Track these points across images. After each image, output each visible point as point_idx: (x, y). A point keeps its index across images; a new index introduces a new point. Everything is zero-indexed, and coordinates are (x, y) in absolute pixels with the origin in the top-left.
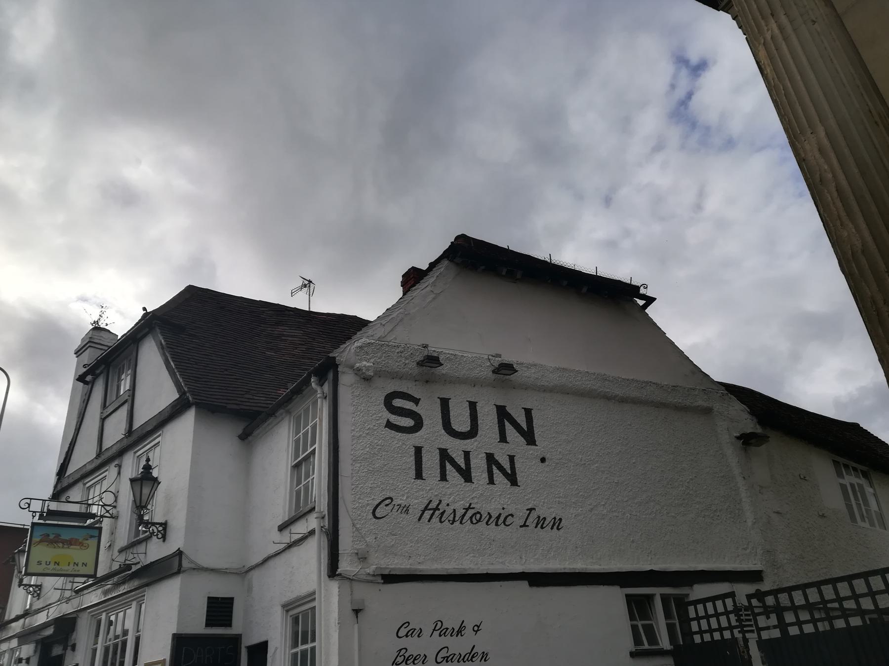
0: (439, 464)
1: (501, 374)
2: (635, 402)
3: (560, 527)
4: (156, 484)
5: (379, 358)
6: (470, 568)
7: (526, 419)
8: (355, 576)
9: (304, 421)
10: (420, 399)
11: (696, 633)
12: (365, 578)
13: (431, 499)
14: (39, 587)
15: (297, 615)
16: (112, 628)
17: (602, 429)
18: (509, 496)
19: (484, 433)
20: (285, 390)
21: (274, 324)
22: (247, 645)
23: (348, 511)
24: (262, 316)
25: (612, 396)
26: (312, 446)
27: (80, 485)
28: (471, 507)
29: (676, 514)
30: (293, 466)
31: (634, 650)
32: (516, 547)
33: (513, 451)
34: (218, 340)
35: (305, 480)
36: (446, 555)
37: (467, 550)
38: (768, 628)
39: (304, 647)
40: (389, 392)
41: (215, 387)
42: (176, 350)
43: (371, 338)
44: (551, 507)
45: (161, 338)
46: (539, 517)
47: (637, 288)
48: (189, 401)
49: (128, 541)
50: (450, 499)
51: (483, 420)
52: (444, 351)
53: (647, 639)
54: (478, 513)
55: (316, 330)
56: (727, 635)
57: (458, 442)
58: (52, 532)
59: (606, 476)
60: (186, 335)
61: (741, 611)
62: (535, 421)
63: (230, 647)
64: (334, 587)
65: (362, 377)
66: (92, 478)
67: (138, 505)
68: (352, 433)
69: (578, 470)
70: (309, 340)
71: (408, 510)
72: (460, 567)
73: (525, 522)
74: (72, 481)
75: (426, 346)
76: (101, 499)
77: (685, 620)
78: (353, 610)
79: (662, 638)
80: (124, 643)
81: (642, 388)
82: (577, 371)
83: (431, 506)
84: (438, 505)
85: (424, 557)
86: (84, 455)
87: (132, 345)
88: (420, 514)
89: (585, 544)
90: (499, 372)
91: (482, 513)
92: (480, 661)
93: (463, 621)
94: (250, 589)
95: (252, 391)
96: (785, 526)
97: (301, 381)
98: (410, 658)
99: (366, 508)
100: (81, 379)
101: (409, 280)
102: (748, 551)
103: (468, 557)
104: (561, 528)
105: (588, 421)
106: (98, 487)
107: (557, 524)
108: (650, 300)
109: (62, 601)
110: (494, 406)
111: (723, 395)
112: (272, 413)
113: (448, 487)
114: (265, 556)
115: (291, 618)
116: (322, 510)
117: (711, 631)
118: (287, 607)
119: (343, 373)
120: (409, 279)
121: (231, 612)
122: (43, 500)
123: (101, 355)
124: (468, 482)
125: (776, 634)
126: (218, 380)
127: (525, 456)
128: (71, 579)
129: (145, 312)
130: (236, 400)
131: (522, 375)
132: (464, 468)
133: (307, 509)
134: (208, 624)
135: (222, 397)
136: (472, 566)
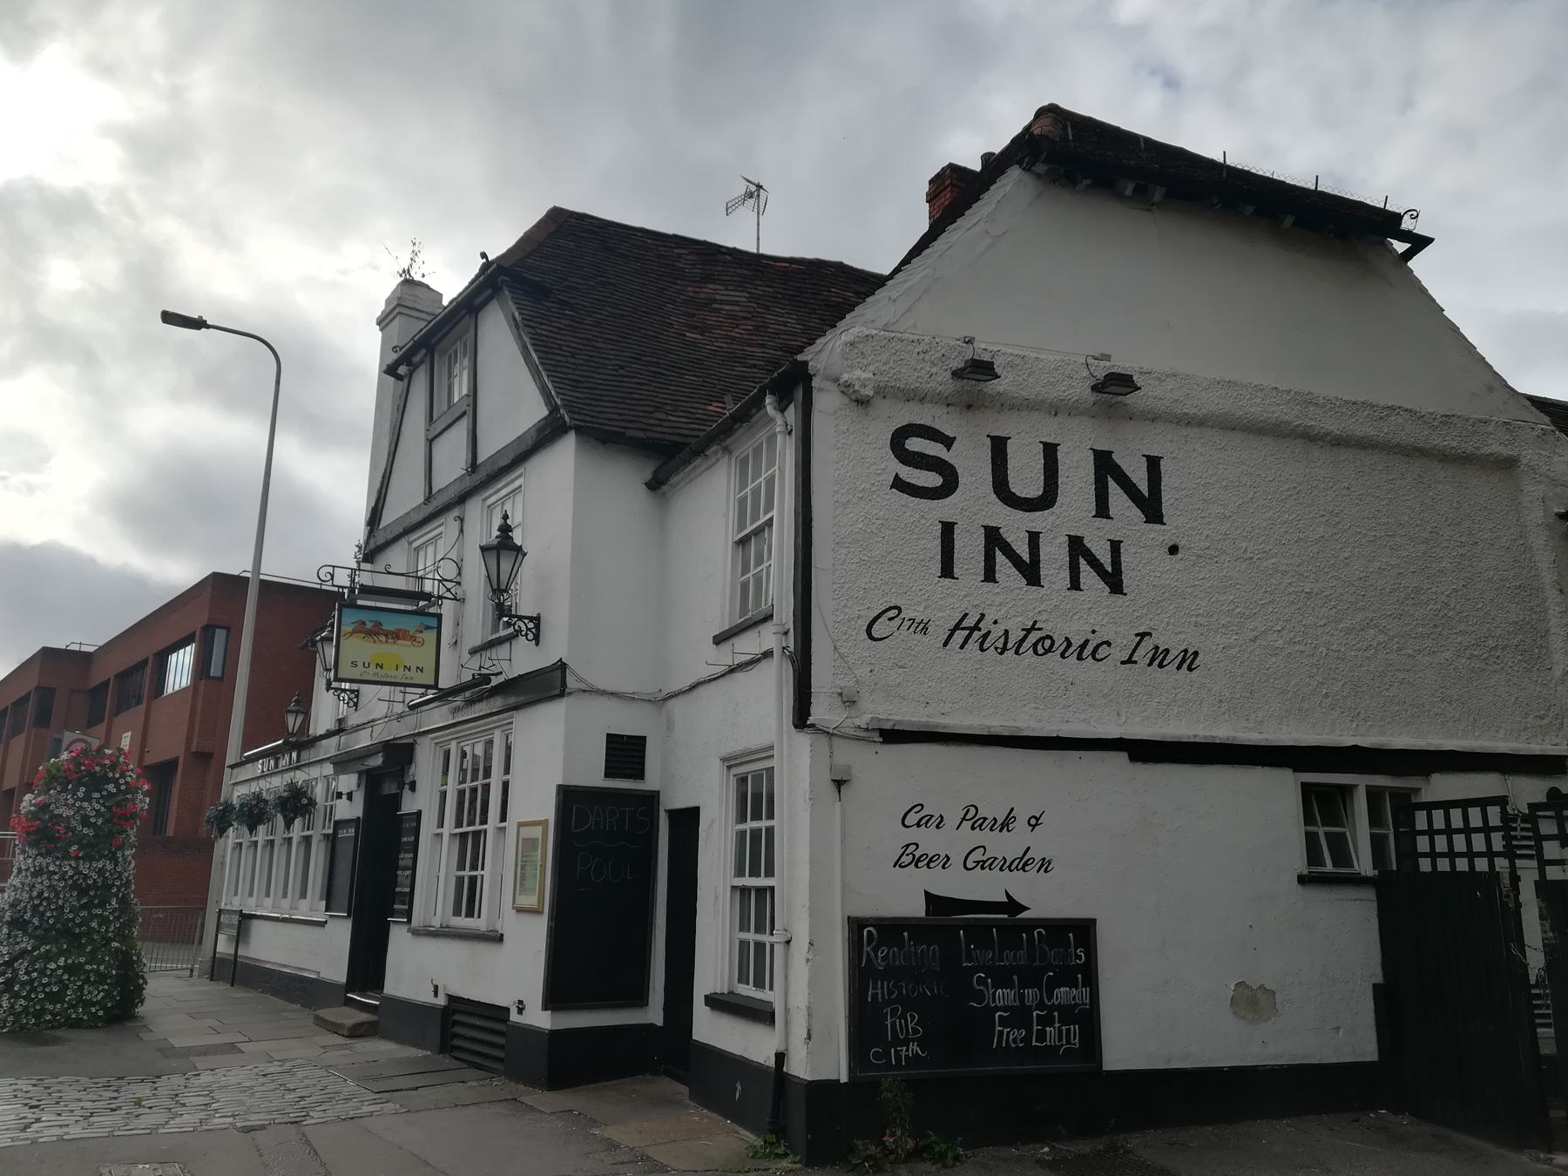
3: (1193, 666)
4: (520, 556)
5: (885, 364)
6: (1029, 726)
7: (1148, 477)
10: (955, 438)
11: (1424, 855)
19: (1068, 500)
21: (698, 279)
22: (667, 808)
23: (826, 627)
25: (1318, 433)
26: (766, 512)
27: (403, 542)
29: (1415, 651)
31: (1305, 872)
32: (1112, 697)
33: (1119, 533)
34: (606, 310)
35: (755, 567)
37: (1026, 697)
39: (756, 824)
42: (539, 331)
44: (1181, 633)
45: (513, 307)
46: (1157, 648)
47: (1398, 218)
48: (565, 422)
49: (482, 640)
51: (1068, 476)
52: (1004, 350)
56: (1482, 865)
57: (1019, 514)
58: (368, 618)
59: (1290, 581)
60: (553, 302)
62: (1165, 480)
64: (803, 740)
65: (854, 397)
67: (495, 587)
68: (833, 496)
69: (1238, 569)
71: (927, 629)
72: (1011, 725)
73: (1132, 655)
75: (969, 341)
76: (437, 570)
77: (1407, 836)
80: (487, 787)
81: (1382, 418)
82: (1256, 386)
83: (967, 623)
84: (979, 621)
85: (950, 705)
86: (406, 499)
89: (1238, 696)
90: (1105, 390)
91: (1054, 638)
92: (1038, 871)
93: (1012, 809)
94: (670, 726)
95: (666, 407)
97: (747, 401)
99: (856, 622)
100: (390, 370)
102: (1546, 721)
106: (430, 550)
107: (1189, 660)
108: (1420, 243)
110: (1091, 451)
111: (1544, 434)
112: (699, 451)
118: (730, 762)
119: (821, 390)
120: (942, 187)
122: (352, 569)
123: (419, 333)
128: (402, 689)
130: (641, 422)
134: (609, 774)
136: (1033, 724)
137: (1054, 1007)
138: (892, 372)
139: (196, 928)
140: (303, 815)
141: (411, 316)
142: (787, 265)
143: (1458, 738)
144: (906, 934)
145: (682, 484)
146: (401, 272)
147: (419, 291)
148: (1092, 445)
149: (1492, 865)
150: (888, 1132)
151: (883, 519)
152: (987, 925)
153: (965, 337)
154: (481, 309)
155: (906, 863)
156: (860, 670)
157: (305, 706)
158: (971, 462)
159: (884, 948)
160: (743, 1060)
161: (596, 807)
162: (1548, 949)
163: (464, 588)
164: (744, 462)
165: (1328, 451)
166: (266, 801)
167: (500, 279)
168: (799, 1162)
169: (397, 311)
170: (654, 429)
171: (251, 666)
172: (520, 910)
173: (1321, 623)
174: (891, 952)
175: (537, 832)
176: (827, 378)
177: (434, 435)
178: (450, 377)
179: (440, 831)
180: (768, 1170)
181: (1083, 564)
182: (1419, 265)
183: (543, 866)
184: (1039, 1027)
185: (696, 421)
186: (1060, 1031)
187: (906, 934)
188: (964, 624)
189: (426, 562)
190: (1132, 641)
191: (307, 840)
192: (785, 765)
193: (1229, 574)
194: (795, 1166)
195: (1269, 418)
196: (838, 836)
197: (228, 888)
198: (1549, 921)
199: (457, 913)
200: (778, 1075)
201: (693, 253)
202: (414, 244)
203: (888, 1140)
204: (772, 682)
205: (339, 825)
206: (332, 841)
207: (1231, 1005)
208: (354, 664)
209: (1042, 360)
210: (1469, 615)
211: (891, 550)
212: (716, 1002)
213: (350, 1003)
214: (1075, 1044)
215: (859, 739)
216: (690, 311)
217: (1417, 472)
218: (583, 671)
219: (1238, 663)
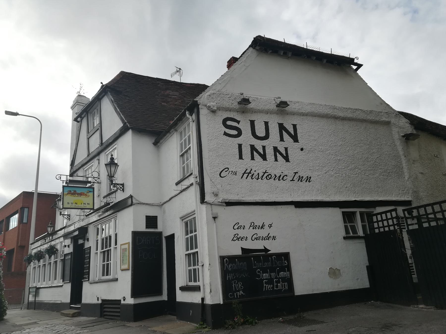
1: (281, 107)
3: (310, 181)
4: (117, 166)
9: (184, 134)
10: (240, 121)
11: (376, 228)
12: (217, 203)
14: (69, 215)
15: (187, 221)
16: (104, 232)
20: (169, 124)
24: (158, 85)
27: (82, 169)
31: (345, 236)
35: (186, 162)
36: (255, 194)
38: (412, 224)
39: (191, 235)
41: (139, 120)
43: (215, 90)
44: (306, 172)
45: (111, 97)
46: (300, 176)
47: (353, 59)
48: (128, 127)
50: (256, 169)
51: (272, 131)
53: (351, 231)
54: (270, 174)
55: (185, 92)
56: (392, 228)
57: (259, 141)
58: (72, 190)
61: (400, 219)
62: (298, 131)
63: (157, 237)
64: (204, 207)
65: (211, 110)
66: (87, 166)
67: (110, 175)
68: (207, 138)
70: (182, 97)
71: (236, 174)
74: (78, 168)
75: (242, 94)
77: (371, 222)
78: (213, 217)
81: (354, 112)
84: (251, 171)
85: (244, 195)
86: (82, 156)
87: (98, 102)
92: (272, 240)
93: (264, 223)
94: (164, 212)
96: (425, 180)
97: (181, 114)
98: (240, 238)
100: (75, 120)
101: (231, 64)
102: (405, 191)
106: (90, 170)
107: (309, 179)
108: (359, 66)
109: (80, 221)
115: (184, 223)
117: (384, 227)
118: (182, 218)
119: (202, 108)
120: (231, 63)
121: (157, 222)
122: (66, 175)
125: (416, 227)
129: (102, 85)
132: (263, 154)
133: (189, 174)
134: (147, 227)
135: (143, 125)
136: (267, 198)
137: (280, 278)
139: (22, 299)
140: (54, 255)
141: (81, 105)
142: (189, 85)
143: (382, 197)
144: (236, 260)
145: (164, 142)
146: (77, 92)
147: (82, 98)
148: (278, 122)
149: (394, 228)
150: (235, 317)
151: (222, 144)
152: (259, 256)
153: (241, 93)
154: (102, 99)
156: (218, 186)
157: (53, 224)
158: (245, 127)
159: (230, 264)
160: (192, 303)
161: (144, 237)
162: (412, 248)
163: (101, 179)
164: (181, 133)
165: (341, 121)
166: (42, 252)
167: (107, 90)
168: (210, 329)
169: (76, 104)
170: (154, 128)
171: (36, 214)
172: (122, 270)
173: (343, 168)
174: (233, 265)
175: (126, 246)
176: (203, 105)
177: (89, 137)
178: (93, 120)
179: (97, 252)
180: (201, 331)
181: (278, 154)
182: (360, 72)
184: (276, 284)
185: (167, 126)
186: (282, 285)
187: (236, 260)
188: (246, 172)
190: (293, 175)
191: (56, 262)
192: (199, 215)
193: (317, 155)
194: (209, 330)
195: (325, 113)
196: (215, 233)
197: (32, 281)
198: (411, 241)
199: (103, 275)
200: (203, 305)
201: (162, 82)
202: (81, 84)
203: (236, 319)
204: (194, 192)
205: (66, 255)
206: (63, 261)
207: (328, 275)
208: (68, 203)
209: (262, 99)
210: (382, 164)
212: (183, 289)
213: (71, 308)
214: (286, 288)
215: (220, 205)
216: (162, 97)
217: (365, 126)
218: (138, 197)
219: (322, 179)
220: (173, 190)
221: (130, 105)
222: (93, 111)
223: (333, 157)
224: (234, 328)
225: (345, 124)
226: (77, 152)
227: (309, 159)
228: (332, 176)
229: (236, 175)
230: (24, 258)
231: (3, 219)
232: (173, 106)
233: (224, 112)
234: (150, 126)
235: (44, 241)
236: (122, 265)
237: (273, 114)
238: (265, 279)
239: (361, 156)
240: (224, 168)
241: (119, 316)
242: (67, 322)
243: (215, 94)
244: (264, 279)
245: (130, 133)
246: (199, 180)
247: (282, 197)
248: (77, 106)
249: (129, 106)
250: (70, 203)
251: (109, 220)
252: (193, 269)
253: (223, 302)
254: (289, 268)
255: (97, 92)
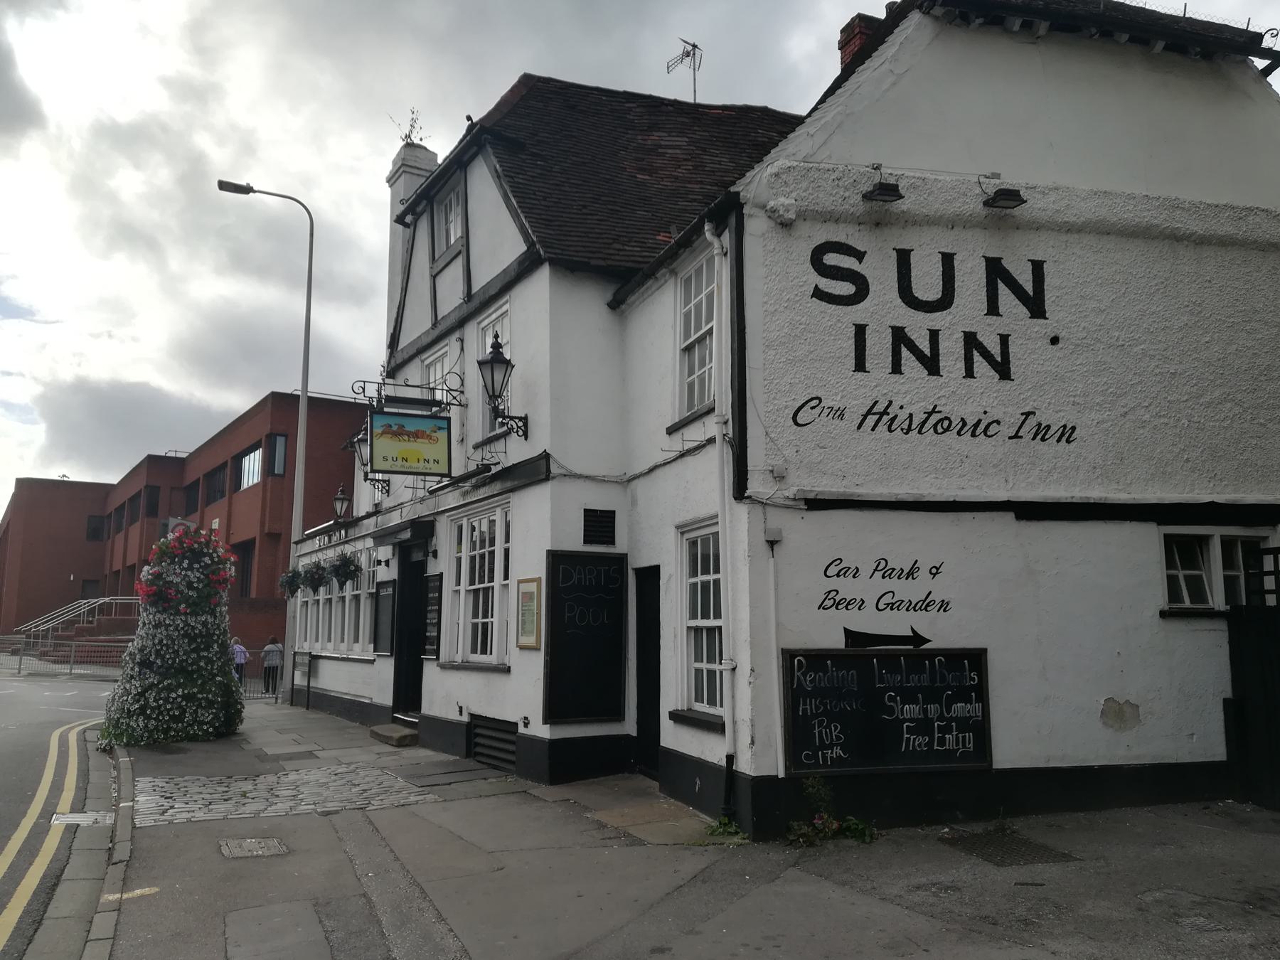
0: (891, 349)
2: (1225, 242)
3: (1071, 439)
4: (509, 368)
5: (804, 191)
8: (770, 499)
9: (695, 289)
10: (866, 252)
13: (877, 399)
17: (1159, 289)
18: (995, 395)
21: (645, 128)
22: (635, 567)
24: (628, 116)
27: (417, 362)
28: (936, 410)
30: (683, 349)
31: (1167, 608)
32: (1001, 466)
37: (927, 469)
40: (819, 243)
43: (793, 158)
44: (1060, 411)
45: (494, 161)
46: (1039, 425)
48: (540, 255)
50: (905, 400)
51: (963, 281)
55: (707, 134)
57: (920, 316)
64: (742, 510)
65: (779, 221)
67: (491, 393)
71: (844, 415)
77: (1256, 576)
78: (767, 541)
79: (1214, 595)
81: (1241, 218)
83: (877, 409)
84: (888, 407)
85: (863, 478)
86: (417, 325)
87: (458, 171)
88: (861, 419)
92: (938, 611)
93: (916, 561)
94: (634, 502)
95: (621, 238)
100: (399, 220)
103: (927, 479)
104: (1072, 441)
105: (1137, 277)
106: (439, 366)
107: (1067, 434)
113: (904, 382)
114: (651, 464)
115: (688, 542)
116: (724, 413)
118: (682, 529)
119: (751, 216)
121: (613, 527)
124: (934, 375)
126: (576, 246)
127: (1026, 335)
128: (423, 477)
131: (1035, 207)
132: (929, 355)
134: (588, 540)
137: (952, 719)
138: (811, 197)
140: (353, 579)
144: (829, 662)
145: (637, 303)
153: (873, 164)
154: (468, 165)
155: (829, 606)
156: (788, 452)
157: (349, 495)
164: (687, 282)
166: (324, 569)
167: (483, 137)
172: (522, 648)
173: (1185, 399)
174: (817, 676)
175: (532, 587)
179: (457, 588)
180: (724, 844)
183: (539, 614)
184: (940, 735)
186: (957, 738)
187: (829, 662)
189: (436, 374)
194: (744, 841)
195: (1140, 223)
196: (772, 586)
199: (474, 651)
200: (729, 771)
202: (413, 113)
203: (818, 822)
204: (716, 465)
205: (380, 585)
206: (375, 597)
207: (1101, 717)
208: (385, 459)
211: (812, 349)
212: (676, 717)
213: (396, 720)
215: (788, 507)
218: (564, 459)
220: (662, 446)
221: (547, 186)
222: (446, 198)
223: (1153, 364)
224: (811, 844)
225: (1206, 257)
226: (405, 311)
227: (1074, 370)
228: (1143, 425)
229: (842, 419)
230: (281, 579)
231: (225, 460)
232: (669, 184)
233: (819, 226)
234: (601, 252)
235: (326, 538)
236: (522, 635)
237: (970, 227)
238: (908, 721)
239: (1248, 361)
240: (807, 399)
241: (512, 762)
242: (386, 760)
243: (792, 171)
244: (905, 720)
245: (544, 274)
246: (731, 430)
247: (978, 486)
248: (403, 176)
249: (543, 187)
250: (390, 459)
251: (489, 509)
252: (708, 671)
253: (786, 774)
254: (981, 693)
255: (456, 143)
